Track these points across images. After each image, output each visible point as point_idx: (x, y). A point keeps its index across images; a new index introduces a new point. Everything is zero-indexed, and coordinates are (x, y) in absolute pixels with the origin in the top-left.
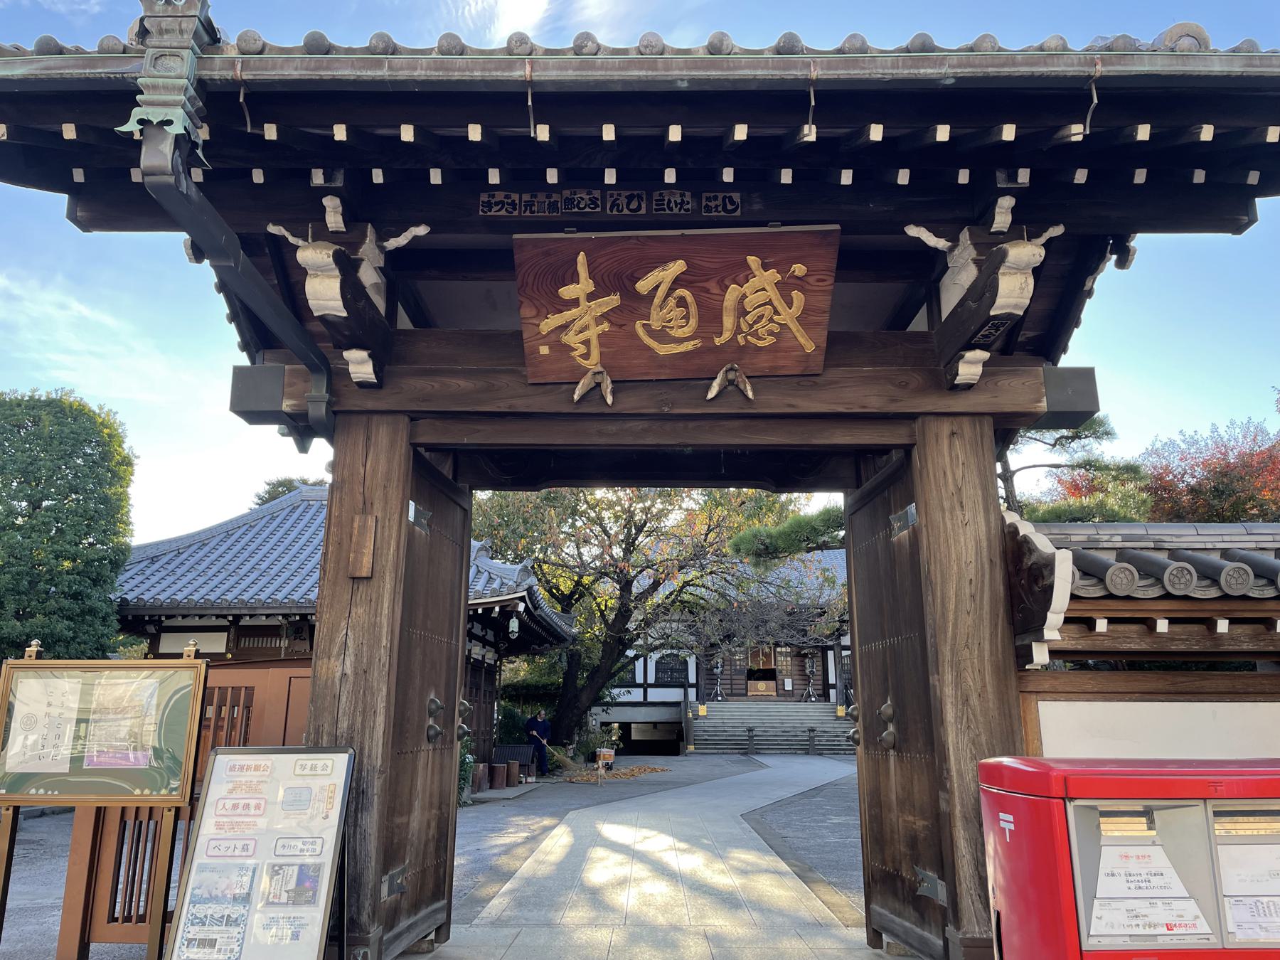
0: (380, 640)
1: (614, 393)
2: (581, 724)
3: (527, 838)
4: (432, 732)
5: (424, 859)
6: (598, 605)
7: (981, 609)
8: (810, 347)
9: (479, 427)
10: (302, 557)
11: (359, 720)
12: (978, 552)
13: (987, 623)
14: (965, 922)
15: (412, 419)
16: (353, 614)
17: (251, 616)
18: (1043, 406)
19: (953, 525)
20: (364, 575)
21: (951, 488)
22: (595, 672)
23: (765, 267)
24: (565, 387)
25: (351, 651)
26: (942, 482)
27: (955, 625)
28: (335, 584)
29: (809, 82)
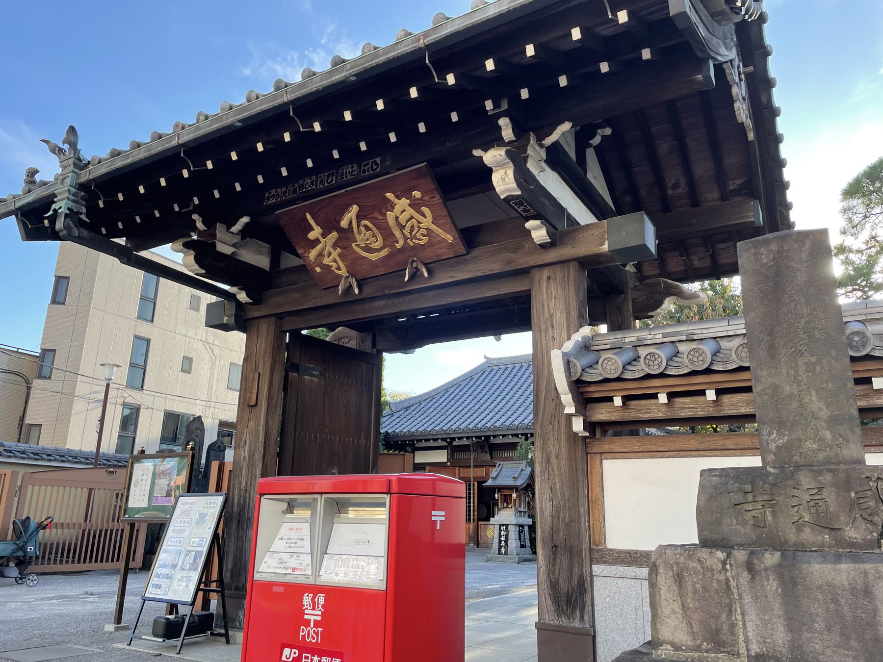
8: (450, 238)
21: (547, 314)
23: (399, 197)
29: (285, 104)
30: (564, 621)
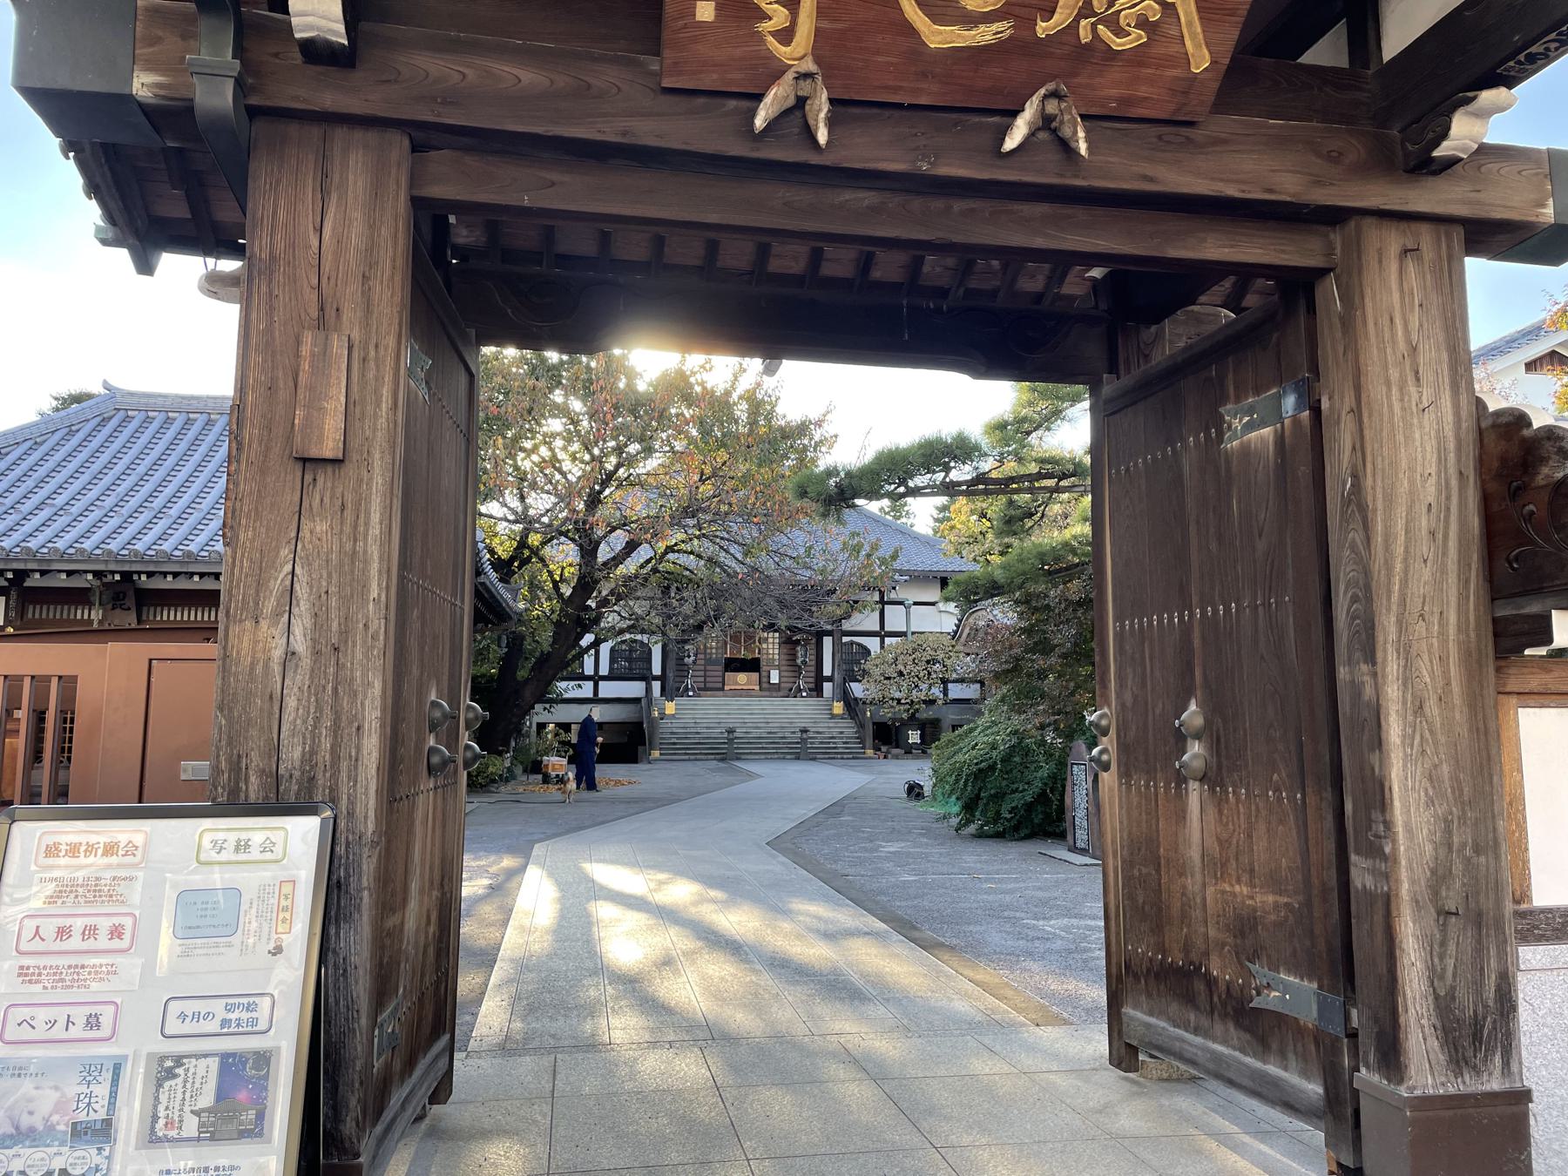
0: (365, 586)
1: (831, 123)
2: (518, 731)
3: (491, 887)
4: (435, 760)
5: (422, 976)
6: (551, 573)
7: (1445, 554)
9: (554, 176)
10: (121, 490)
11: (326, 744)
12: (1442, 461)
13: (1452, 578)
14: (1412, 1070)
15: (415, 148)
16: (305, 532)
17: (43, 573)
18: (1548, 214)
19: (1403, 409)
20: (328, 454)
21: (1402, 345)
22: (544, 660)
24: (732, 104)
25: (303, 607)
26: (1387, 335)
27: (1405, 582)
28: (263, 472)
30: (1469, 1084)
